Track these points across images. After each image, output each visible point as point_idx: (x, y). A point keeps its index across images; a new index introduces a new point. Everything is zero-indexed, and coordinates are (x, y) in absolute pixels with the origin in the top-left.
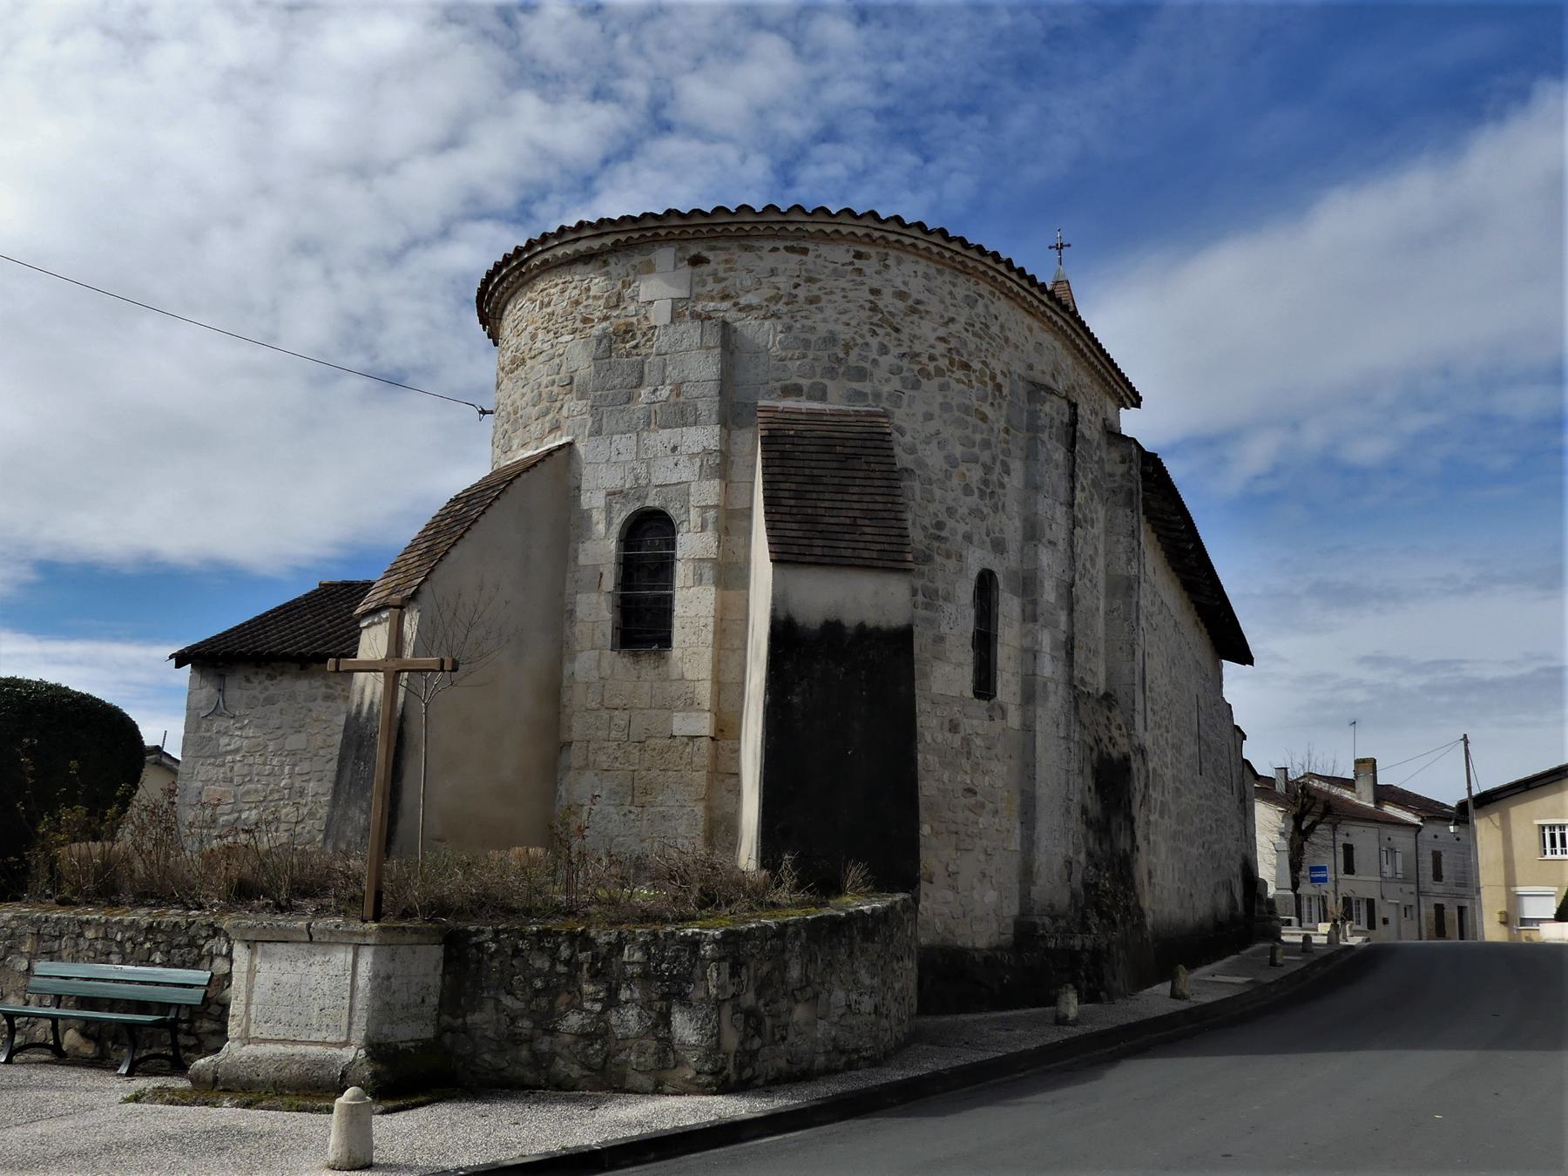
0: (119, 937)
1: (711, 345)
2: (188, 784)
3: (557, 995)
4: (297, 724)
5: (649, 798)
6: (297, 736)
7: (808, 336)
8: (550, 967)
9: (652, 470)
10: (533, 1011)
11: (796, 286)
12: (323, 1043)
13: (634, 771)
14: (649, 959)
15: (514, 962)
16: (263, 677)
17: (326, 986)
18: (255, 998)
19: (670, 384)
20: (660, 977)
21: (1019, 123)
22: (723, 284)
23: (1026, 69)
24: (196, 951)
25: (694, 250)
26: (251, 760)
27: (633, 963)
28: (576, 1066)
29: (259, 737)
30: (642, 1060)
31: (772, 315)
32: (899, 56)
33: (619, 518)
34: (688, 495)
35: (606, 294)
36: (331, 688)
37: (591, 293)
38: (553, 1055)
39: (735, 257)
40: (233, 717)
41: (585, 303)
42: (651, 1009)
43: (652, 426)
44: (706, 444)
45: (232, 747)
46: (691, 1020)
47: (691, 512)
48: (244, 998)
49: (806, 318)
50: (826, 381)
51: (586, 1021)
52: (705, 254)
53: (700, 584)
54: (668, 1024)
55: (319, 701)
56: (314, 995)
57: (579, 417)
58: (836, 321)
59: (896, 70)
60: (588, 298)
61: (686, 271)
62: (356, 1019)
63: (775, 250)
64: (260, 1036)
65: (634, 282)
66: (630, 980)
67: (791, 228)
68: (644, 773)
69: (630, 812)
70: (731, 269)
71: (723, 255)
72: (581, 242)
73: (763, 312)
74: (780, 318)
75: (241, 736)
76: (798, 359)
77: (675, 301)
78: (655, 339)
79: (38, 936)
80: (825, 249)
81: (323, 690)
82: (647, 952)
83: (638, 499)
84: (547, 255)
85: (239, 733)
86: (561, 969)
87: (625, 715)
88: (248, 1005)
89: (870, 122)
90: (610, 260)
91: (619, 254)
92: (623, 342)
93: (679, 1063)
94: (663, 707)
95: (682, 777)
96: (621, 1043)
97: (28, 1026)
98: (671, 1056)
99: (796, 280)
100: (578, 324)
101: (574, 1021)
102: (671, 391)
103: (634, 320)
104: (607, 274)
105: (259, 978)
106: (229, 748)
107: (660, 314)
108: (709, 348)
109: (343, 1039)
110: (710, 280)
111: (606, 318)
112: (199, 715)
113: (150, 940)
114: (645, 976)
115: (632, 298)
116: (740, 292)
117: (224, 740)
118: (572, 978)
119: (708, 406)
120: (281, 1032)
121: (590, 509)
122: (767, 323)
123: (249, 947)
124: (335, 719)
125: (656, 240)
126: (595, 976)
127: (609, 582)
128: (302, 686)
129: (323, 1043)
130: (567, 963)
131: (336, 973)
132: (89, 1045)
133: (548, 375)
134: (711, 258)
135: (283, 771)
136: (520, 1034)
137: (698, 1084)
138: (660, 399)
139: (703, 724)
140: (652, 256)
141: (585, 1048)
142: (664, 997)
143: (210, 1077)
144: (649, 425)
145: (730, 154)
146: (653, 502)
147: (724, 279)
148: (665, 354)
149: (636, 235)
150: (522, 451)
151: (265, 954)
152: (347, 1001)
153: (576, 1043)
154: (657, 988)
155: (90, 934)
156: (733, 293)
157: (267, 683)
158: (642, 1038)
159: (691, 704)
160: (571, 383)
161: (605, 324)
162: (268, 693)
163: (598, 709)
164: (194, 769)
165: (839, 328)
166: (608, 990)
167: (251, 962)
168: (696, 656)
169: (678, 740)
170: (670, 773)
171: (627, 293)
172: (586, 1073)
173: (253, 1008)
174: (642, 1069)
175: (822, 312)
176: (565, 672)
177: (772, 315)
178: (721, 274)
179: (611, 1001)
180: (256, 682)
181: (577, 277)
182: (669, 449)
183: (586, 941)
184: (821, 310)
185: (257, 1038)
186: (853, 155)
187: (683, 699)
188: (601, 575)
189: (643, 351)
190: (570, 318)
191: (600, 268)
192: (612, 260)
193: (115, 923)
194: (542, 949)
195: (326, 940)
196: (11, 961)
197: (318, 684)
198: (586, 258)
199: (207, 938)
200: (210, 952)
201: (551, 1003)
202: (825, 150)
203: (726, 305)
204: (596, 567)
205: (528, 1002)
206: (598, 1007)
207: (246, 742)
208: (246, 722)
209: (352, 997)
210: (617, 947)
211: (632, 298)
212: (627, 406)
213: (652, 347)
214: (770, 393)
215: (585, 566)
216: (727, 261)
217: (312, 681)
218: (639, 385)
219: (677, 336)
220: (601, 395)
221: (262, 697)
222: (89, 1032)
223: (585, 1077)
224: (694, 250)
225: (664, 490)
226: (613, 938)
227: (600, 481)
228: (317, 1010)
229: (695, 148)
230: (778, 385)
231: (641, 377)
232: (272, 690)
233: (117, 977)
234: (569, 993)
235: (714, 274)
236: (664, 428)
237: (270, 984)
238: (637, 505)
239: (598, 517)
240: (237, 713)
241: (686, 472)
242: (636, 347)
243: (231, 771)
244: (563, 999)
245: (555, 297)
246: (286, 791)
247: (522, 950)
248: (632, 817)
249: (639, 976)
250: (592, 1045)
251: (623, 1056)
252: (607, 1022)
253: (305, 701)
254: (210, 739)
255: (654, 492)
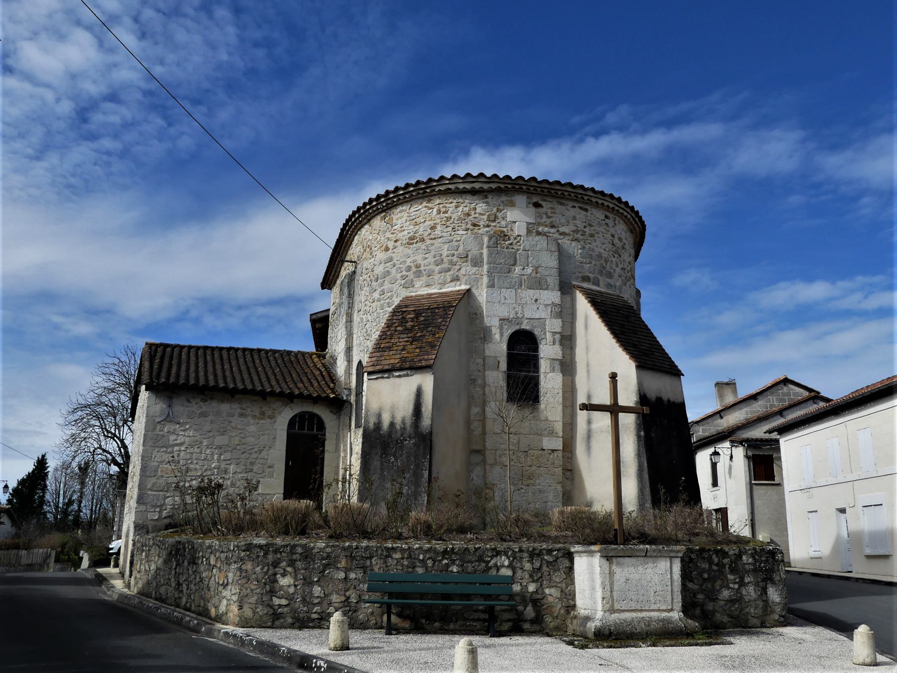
0: (421, 557)
1: (553, 250)
2: (148, 463)
3: (715, 581)
4: (222, 430)
5: (532, 481)
6: (222, 437)
7: (591, 253)
8: (709, 567)
9: (525, 310)
10: (704, 590)
11: (585, 227)
12: (659, 610)
13: (522, 466)
14: (755, 561)
15: (690, 565)
16: (198, 400)
17: (656, 579)
18: (615, 588)
19: (532, 267)
20: (761, 570)
21: (224, 115)
22: (551, 220)
23: (232, 87)
24: (484, 565)
25: (535, 199)
26: (192, 450)
27: (748, 564)
28: (725, 617)
29: (197, 436)
30: (756, 611)
31: (576, 240)
32: (162, 63)
33: (507, 334)
34: (545, 325)
35: (487, 214)
36: (244, 409)
37: (477, 211)
38: (714, 611)
39: (556, 207)
40: (179, 424)
41: (473, 216)
42: (759, 586)
43: (523, 287)
44: (553, 300)
45: (178, 442)
46: (776, 591)
47: (547, 334)
48: (609, 588)
49: (590, 244)
50: (599, 276)
51: (732, 593)
52: (541, 202)
53: (553, 372)
54: (766, 593)
55: (236, 417)
56: (650, 585)
57: (473, 276)
58: (601, 247)
59: (158, 70)
60: (475, 213)
61: (532, 209)
62: (675, 597)
63: (574, 207)
64: (621, 609)
65: (503, 210)
66: (748, 572)
67: (586, 198)
68: (528, 468)
69: (522, 488)
70: (554, 213)
71: (549, 205)
72: (476, 183)
73: (571, 237)
74: (579, 242)
75: (184, 435)
76: (588, 264)
77: (528, 224)
78: (521, 242)
79: (352, 558)
80: (594, 211)
81: (239, 410)
82: (754, 558)
83: (517, 324)
84: (450, 186)
85: (183, 433)
86: (715, 568)
87: (516, 437)
88: (611, 592)
89: (139, 96)
90: (488, 196)
91: (494, 194)
92: (504, 240)
93: (772, 612)
94: (537, 434)
95: (549, 471)
96: (747, 603)
97: (351, 613)
98: (769, 609)
99: (585, 224)
100: (469, 226)
101: (726, 594)
102: (533, 270)
103: (505, 229)
104: (487, 203)
105: (617, 577)
106: (176, 442)
107: (519, 229)
108: (551, 251)
109: (670, 607)
110: (544, 216)
111: (488, 226)
112: (155, 420)
113: (447, 559)
114: (755, 570)
115: (503, 218)
116: (560, 226)
117: (172, 438)
118: (721, 571)
119: (553, 280)
120: (633, 605)
121: (491, 327)
122: (573, 243)
123: (608, 560)
124: (247, 428)
125: (520, 191)
126: (733, 571)
127: (504, 366)
128: (225, 407)
129: (659, 610)
130: (717, 565)
131: (661, 572)
132: (405, 622)
133: (448, 250)
134: (544, 205)
135: (213, 457)
136: (698, 602)
137: (780, 622)
138: (527, 273)
139: (558, 444)
140: (513, 198)
141: (731, 606)
142: (764, 580)
143: (607, 632)
144: (521, 286)
145: (50, 96)
146: (525, 326)
147: (551, 217)
148: (528, 251)
149: (510, 186)
150: (426, 289)
151: (618, 564)
152: (669, 588)
153: (726, 605)
154: (761, 576)
155: (398, 556)
156: (556, 225)
157: (201, 404)
158: (756, 600)
159: (552, 433)
160: (467, 257)
161: (487, 229)
162: (201, 410)
163: (501, 433)
164: (152, 454)
165: (602, 251)
166: (740, 577)
167: (610, 568)
168: (554, 409)
169: (546, 452)
170: (542, 469)
171: (499, 215)
172: (730, 620)
173: (615, 593)
174: (756, 616)
175: (595, 242)
176: (472, 412)
177: (576, 240)
178: (550, 214)
179: (742, 584)
180: (194, 402)
181: (467, 201)
182: (533, 301)
183: (725, 554)
184: (595, 240)
185: (619, 609)
186: (127, 113)
187: (547, 430)
188: (499, 362)
189: (516, 247)
190: (463, 222)
191: (483, 199)
192: (490, 196)
193: (416, 549)
194: (703, 558)
195: (655, 555)
196: (329, 573)
197: (235, 407)
198: (473, 192)
199: (492, 557)
200: (496, 565)
201: (713, 585)
202: (109, 106)
203: (553, 230)
204: (496, 357)
205: (701, 585)
206: (736, 586)
207: (187, 439)
208: (188, 427)
209: (672, 585)
210: (739, 556)
211: (503, 218)
212: (509, 275)
213: (520, 246)
214: (577, 278)
215: (489, 357)
216: (552, 208)
217: (232, 405)
218: (515, 264)
219: (534, 242)
220: (493, 267)
221: (198, 412)
222: (404, 614)
223: (729, 621)
224: (535, 199)
225: (532, 321)
226: (737, 552)
227: (495, 312)
228: (652, 593)
229: (27, 87)
230: (580, 275)
231: (515, 260)
232: (205, 408)
233: (471, 581)
234: (721, 580)
235: (546, 214)
236: (530, 289)
237: (623, 580)
238: (517, 328)
239: (496, 332)
240: (181, 421)
241: (544, 313)
242: (511, 244)
243: (178, 456)
244: (719, 583)
245: (451, 209)
246: (215, 470)
247: (693, 559)
248: (523, 491)
249: (752, 570)
250: (733, 605)
251: (747, 610)
252: (741, 594)
253: (227, 416)
254: (163, 436)
255: (526, 321)
